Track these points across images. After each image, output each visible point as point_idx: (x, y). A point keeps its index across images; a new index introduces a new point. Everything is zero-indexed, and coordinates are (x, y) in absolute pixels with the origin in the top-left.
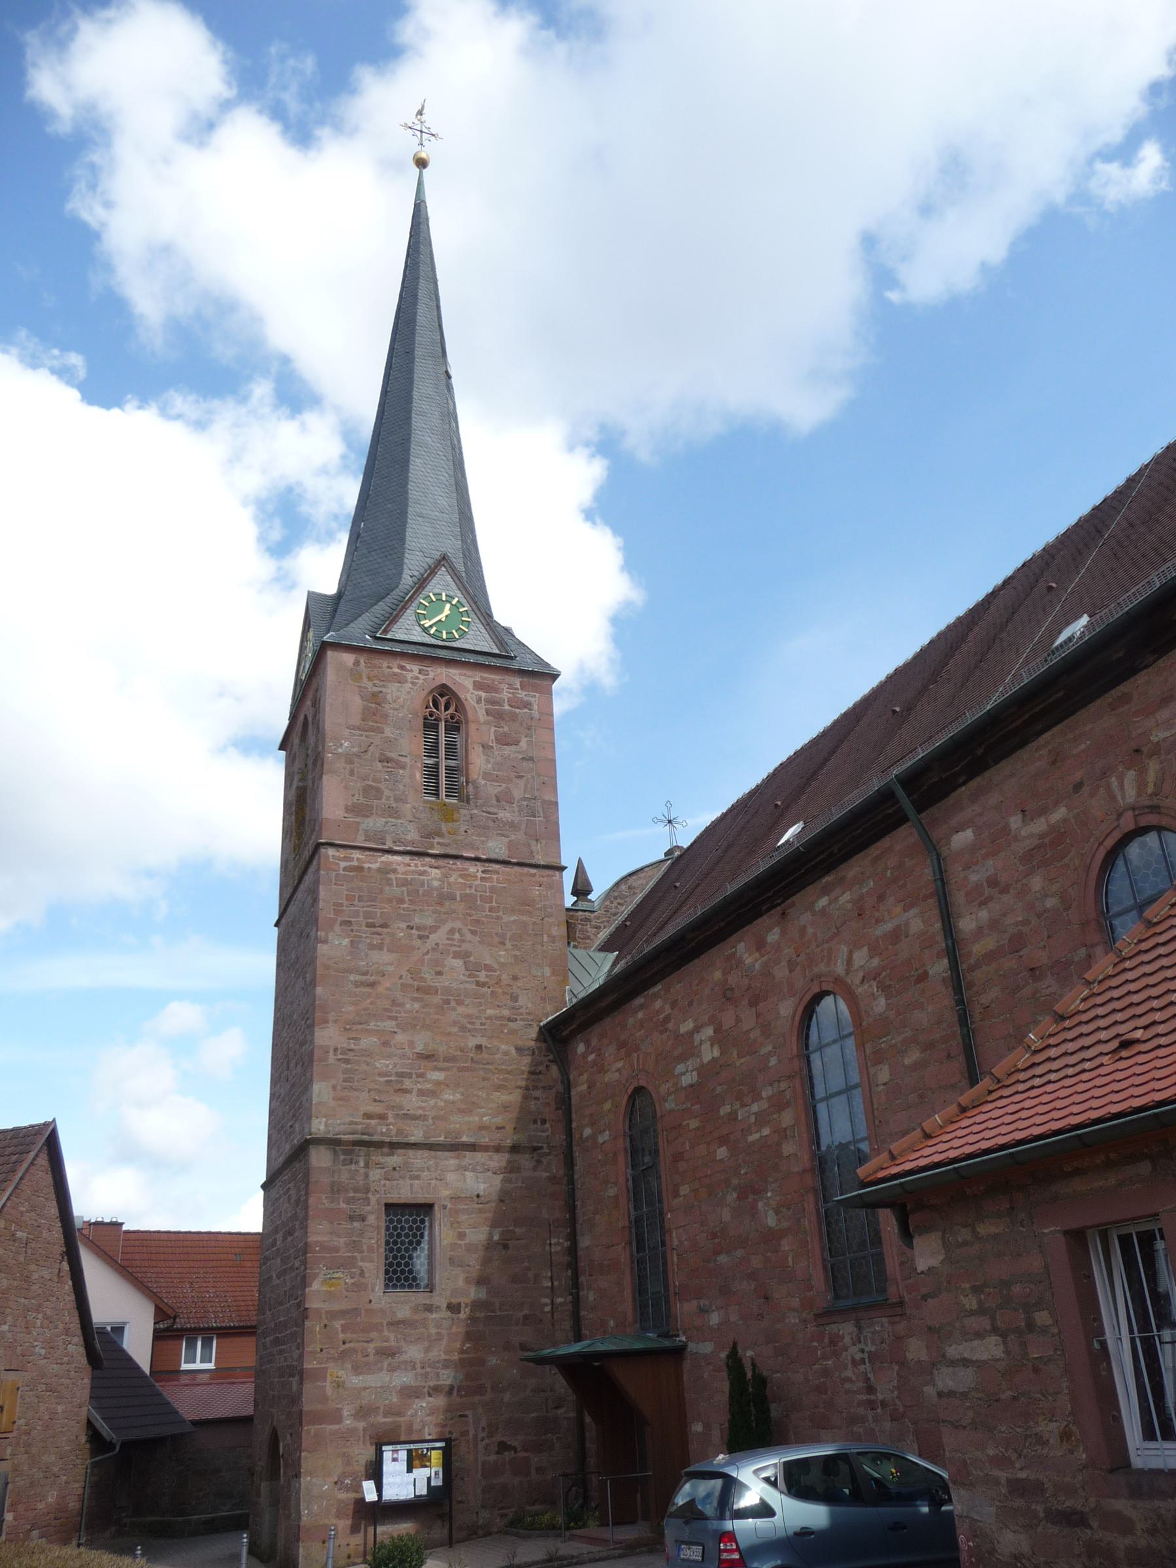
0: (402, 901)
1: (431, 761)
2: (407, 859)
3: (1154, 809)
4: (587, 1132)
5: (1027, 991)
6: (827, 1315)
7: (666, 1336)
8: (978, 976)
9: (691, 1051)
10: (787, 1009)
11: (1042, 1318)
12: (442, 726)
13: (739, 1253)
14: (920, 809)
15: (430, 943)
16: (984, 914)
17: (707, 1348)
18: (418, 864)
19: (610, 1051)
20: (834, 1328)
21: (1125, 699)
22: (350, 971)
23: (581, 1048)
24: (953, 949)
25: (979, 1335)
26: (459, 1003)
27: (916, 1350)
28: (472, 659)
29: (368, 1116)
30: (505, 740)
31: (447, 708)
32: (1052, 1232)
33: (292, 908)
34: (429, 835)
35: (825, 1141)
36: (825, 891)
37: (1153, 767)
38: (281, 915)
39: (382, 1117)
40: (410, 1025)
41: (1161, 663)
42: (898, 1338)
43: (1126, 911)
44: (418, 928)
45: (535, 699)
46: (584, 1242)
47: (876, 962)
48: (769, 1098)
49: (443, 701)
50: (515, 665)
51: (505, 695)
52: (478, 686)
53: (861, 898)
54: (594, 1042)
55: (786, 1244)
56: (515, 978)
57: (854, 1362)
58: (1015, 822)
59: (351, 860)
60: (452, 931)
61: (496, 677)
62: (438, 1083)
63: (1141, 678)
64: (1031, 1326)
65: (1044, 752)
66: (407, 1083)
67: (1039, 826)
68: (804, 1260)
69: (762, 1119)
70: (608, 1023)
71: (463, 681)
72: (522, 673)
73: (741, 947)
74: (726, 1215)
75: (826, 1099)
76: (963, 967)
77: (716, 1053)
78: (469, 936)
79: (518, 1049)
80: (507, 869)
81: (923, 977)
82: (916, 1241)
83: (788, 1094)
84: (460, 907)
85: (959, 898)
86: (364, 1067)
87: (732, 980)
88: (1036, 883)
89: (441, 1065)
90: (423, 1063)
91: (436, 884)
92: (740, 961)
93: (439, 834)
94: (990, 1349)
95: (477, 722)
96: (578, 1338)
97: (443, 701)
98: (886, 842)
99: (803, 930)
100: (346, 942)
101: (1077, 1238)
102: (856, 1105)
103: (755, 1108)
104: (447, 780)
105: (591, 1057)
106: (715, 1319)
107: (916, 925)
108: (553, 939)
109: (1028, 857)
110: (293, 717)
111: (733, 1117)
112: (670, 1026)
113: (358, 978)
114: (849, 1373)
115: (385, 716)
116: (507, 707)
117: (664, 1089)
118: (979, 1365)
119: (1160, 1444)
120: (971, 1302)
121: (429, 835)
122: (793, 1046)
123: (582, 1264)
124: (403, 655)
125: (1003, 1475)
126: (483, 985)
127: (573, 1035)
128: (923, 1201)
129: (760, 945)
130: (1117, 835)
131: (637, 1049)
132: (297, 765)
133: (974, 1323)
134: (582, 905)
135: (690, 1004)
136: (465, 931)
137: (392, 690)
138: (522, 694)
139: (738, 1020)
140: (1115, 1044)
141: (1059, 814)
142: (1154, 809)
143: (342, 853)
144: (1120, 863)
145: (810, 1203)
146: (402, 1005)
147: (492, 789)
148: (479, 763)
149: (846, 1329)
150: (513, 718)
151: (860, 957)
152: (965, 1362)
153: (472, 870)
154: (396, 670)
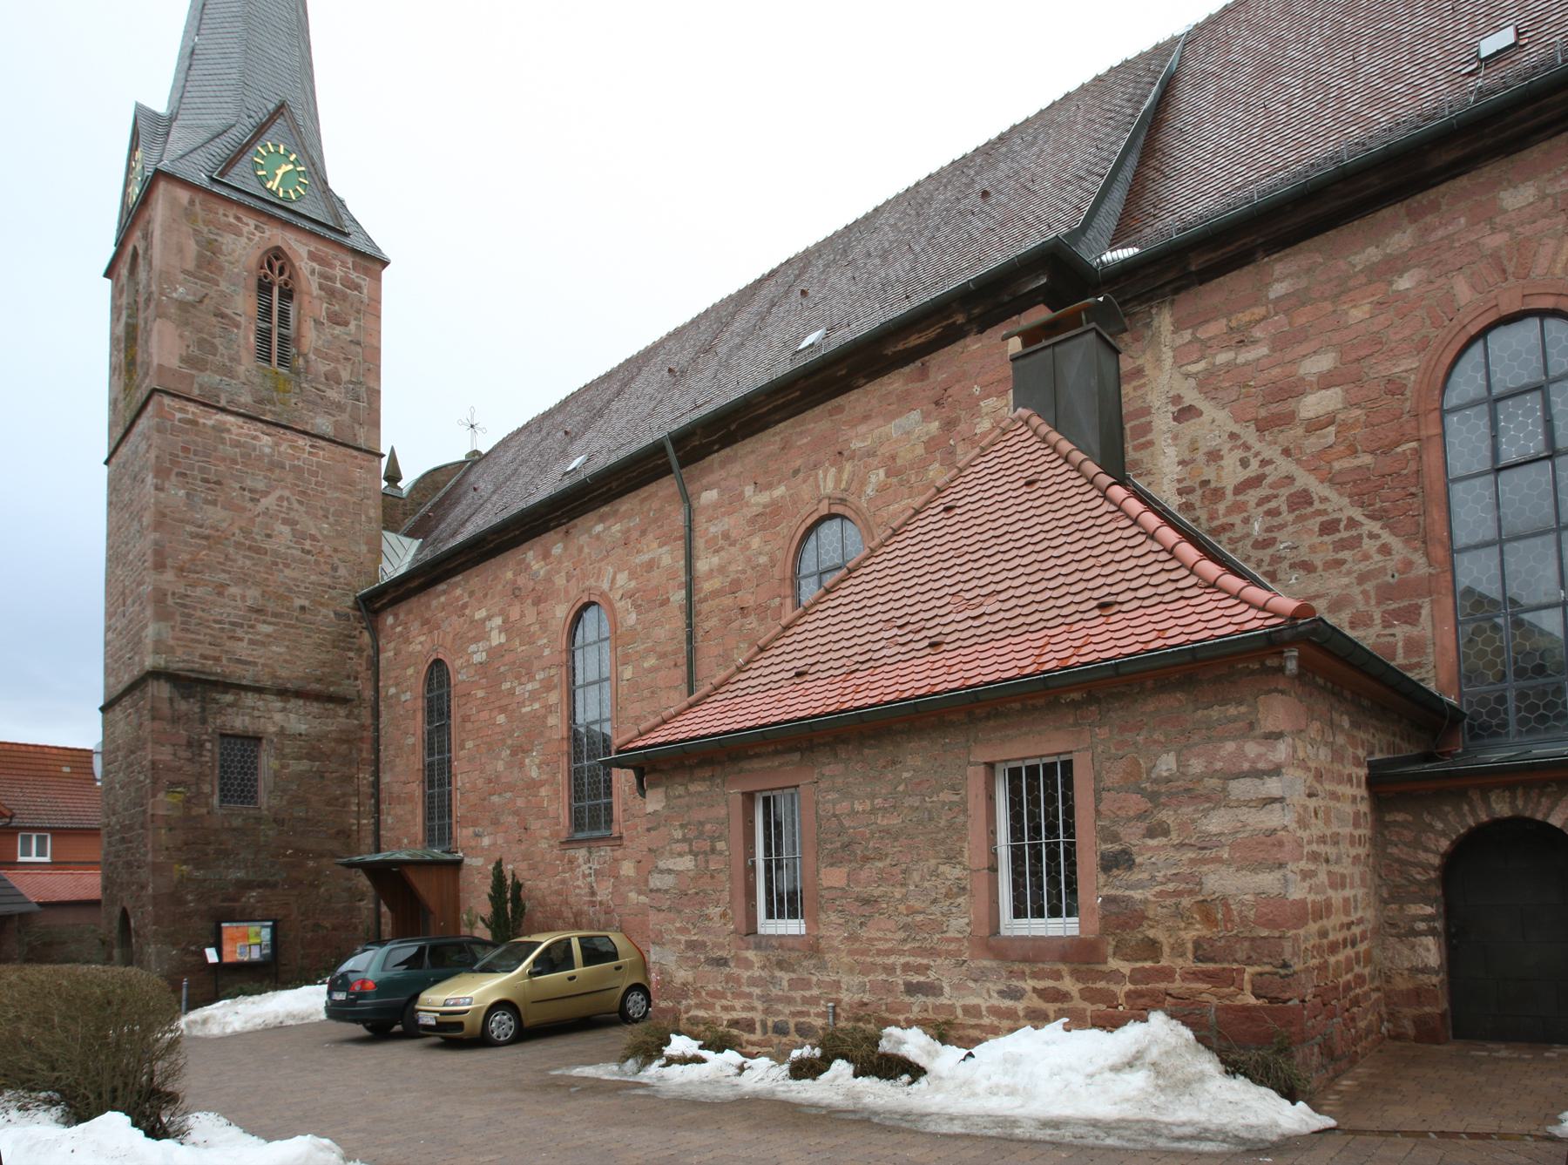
0: (235, 462)
1: (264, 325)
2: (240, 421)
3: (843, 501)
4: (392, 691)
5: (736, 625)
6: (570, 842)
7: (448, 852)
8: (705, 607)
9: (482, 636)
10: (561, 612)
11: (721, 845)
12: (276, 291)
13: (509, 795)
14: (682, 466)
15: (260, 507)
16: (715, 560)
17: (477, 862)
18: (250, 428)
19: (415, 627)
20: (572, 852)
21: (840, 409)
22: (188, 522)
23: (390, 620)
24: (690, 586)
25: (680, 855)
26: (287, 566)
27: (627, 869)
28: (308, 226)
29: (205, 657)
30: (337, 320)
31: (281, 274)
32: (735, 792)
33: (123, 450)
34: (260, 401)
35: (580, 719)
36: (602, 519)
37: (848, 467)
38: (112, 454)
39: (217, 659)
40: (243, 580)
41: (869, 387)
42: (616, 860)
43: (811, 576)
44: (251, 491)
45: (365, 283)
46: (386, 778)
47: (633, 584)
48: (541, 681)
49: (277, 264)
50: (348, 242)
51: (338, 272)
52: (312, 256)
53: (628, 530)
54: (402, 617)
55: (543, 792)
56: (336, 550)
57: (584, 876)
58: (749, 490)
59: (186, 412)
60: (281, 498)
61: (329, 251)
62: (268, 636)
63: (853, 395)
64: (713, 850)
65: (777, 438)
66: (239, 632)
67: (764, 498)
68: (557, 803)
69: (534, 697)
70: (413, 602)
71: (299, 249)
72: (355, 252)
73: (531, 553)
74: (500, 766)
75: (583, 686)
76: (695, 598)
77: (503, 640)
78: (296, 505)
79: (336, 613)
80: (333, 447)
81: (665, 602)
82: (649, 793)
83: (556, 680)
84: (290, 478)
85: (700, 543)
86: (199, 613)
87: (521, 581)
88: (756, 542)
89: (270, 619)
90: (254, 616)
91: (267, 450)
92: (528, 567)
93: (271, 401)
94: (686, 863)
95: (310, 294)
96: (378, 850)
97: (277, 264)
98: (652, 488)
99: (580, 549)
100: (182, 493)
101: (749, 797)
102: (620, 694)
103: (529, 687)
104: (276, 346)
105: (399, 629)
106: (486, 841)
107: (666, 560)
108: (370, 520)
109: (753, 520)
110: (121, 244)
111: (511, 692)
112: (467, 612)
113: (194, 529)
114: (579, 883)
115: (221, 269)
116: (338, 285)
117: (458, 663)
118: (678, 873)
119: (776, 921)
120: (678, 834)
121: (260, 401)
122: (563, 641)
123: (383, 795)
124: (239, 204)
125: (683, 938)
126: (309, 552)
127: (383, 608)
128: (652, 766)
129: (546, 556)
130: (815, 517)
131: (438, 628)
132: (124, 301)
133: (678, 847)
134: (394, 492)
135: (485, 595)
136: (293, 499)
137: (227, 240)
138: (354, 275)
139: (522, 615)
140: (793, 673)
141: (780, 491)
142: (843, 501)
143: (177, 403)
144: (813, 537)
145: (564, 763)
146: (234, 561)
147: (322, 367)
148: (311, 338)
149: (581, 853)
150: (345, 297)
151: (622, 578)
152: (670, 871)
153: (301, 443)
154: (232, 220)
